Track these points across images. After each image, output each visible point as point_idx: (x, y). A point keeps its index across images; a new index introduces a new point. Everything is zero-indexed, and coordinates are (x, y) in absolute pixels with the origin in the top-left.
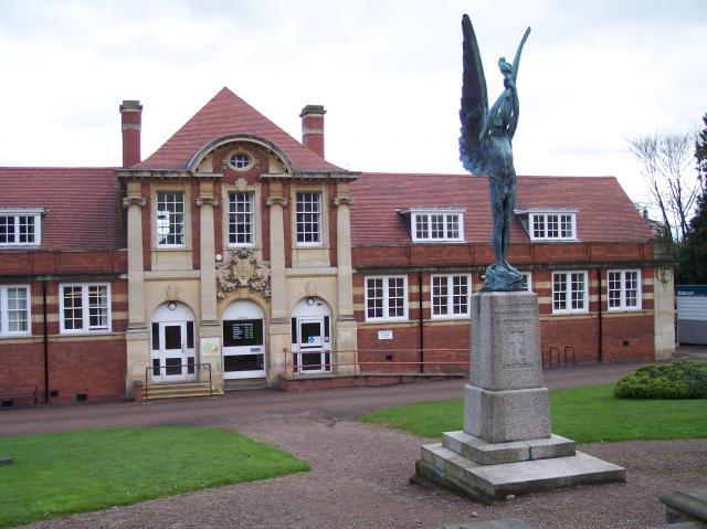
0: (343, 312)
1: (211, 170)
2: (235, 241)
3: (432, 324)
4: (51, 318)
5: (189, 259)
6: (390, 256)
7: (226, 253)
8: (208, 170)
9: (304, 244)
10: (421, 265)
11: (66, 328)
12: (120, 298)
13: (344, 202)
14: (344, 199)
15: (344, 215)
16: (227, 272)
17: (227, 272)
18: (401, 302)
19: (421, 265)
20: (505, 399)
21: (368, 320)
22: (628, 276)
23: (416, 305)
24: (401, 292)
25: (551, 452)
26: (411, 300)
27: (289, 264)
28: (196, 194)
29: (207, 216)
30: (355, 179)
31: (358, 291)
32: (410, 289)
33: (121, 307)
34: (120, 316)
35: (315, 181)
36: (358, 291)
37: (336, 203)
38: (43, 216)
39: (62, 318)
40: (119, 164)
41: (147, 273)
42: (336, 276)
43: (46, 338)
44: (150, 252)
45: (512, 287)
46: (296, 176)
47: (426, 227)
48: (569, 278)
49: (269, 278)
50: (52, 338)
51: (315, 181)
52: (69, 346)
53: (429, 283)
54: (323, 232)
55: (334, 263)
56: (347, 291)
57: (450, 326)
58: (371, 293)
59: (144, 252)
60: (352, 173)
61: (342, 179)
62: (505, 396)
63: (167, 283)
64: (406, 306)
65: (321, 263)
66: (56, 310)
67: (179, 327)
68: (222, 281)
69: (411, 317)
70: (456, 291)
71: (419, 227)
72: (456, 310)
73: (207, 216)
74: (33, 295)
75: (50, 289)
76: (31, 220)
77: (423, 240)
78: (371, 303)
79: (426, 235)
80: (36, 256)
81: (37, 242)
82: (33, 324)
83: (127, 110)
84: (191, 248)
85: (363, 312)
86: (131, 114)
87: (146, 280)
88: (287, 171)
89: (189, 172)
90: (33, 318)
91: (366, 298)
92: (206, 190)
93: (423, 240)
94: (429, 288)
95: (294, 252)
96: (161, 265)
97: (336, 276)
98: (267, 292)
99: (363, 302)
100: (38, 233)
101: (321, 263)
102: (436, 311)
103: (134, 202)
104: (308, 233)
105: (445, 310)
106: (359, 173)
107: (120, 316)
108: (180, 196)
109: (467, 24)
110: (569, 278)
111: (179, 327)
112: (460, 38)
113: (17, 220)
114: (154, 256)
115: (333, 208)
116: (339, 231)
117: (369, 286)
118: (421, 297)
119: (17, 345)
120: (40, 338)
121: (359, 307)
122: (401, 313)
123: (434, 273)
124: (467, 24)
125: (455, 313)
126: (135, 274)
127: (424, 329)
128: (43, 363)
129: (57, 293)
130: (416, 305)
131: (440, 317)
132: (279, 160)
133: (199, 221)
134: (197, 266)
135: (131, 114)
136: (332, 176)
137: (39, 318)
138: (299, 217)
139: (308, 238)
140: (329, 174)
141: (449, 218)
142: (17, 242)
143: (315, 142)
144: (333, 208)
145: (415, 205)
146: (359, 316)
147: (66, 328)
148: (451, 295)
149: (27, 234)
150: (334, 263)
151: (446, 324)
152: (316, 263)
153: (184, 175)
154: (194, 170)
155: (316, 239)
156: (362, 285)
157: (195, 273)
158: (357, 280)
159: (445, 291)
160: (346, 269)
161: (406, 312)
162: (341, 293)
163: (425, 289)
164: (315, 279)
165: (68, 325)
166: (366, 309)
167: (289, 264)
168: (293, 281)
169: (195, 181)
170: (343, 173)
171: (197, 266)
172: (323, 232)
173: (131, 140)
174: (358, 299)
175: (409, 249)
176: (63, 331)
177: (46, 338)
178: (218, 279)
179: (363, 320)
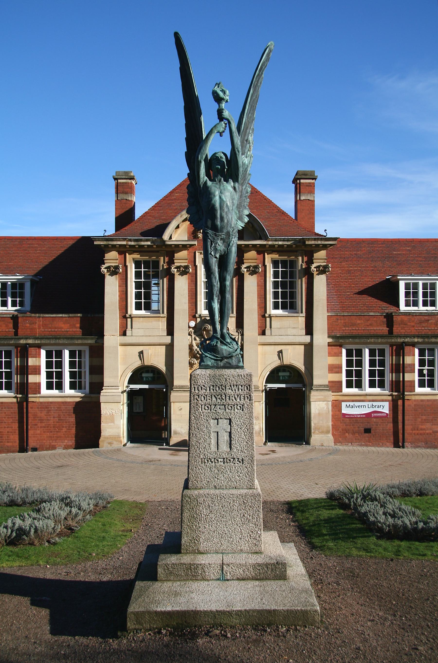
3: (413, 398)
11: (370, 387)
13: (322, 270)
15: (320, 283)
18: (382, 374)
20: (201, 500)
21: (345, 390)
25: (251, 573)
39: (43, 379)
45: (221, 364)
48: (66, 353)
50: (32, 398)
52: (46, 406)
55: (309, 330)
58: (349, 363)
62: (199, 496)
65: (294, 332)
66: (37, 370)
67: (370, 387)
68: (195, 347)
71: (407, 294)
75: (32, 350)
77: (412, 309)
78: (349, 373)
85: (341, 382)
86: (123, 186)
91: (417, 367)
93: (412, 309)
101: (294, 332)
102: (349, 385)
107: (96, 379)
109: (176, 35)
110: (66, 353)
111: (370, 387)
124: (176, 35)
129: (39, 356)
135: (123, 186)
143: (305, 208)
145: (403, 274)
147: (370, 387)
152: (290, 331)
161: (387, 384)
163: (408, 360)
165: (49, 386)
166: (417, 378)
176: (44, 391)
178: (191, 347)
179: (340, 389)
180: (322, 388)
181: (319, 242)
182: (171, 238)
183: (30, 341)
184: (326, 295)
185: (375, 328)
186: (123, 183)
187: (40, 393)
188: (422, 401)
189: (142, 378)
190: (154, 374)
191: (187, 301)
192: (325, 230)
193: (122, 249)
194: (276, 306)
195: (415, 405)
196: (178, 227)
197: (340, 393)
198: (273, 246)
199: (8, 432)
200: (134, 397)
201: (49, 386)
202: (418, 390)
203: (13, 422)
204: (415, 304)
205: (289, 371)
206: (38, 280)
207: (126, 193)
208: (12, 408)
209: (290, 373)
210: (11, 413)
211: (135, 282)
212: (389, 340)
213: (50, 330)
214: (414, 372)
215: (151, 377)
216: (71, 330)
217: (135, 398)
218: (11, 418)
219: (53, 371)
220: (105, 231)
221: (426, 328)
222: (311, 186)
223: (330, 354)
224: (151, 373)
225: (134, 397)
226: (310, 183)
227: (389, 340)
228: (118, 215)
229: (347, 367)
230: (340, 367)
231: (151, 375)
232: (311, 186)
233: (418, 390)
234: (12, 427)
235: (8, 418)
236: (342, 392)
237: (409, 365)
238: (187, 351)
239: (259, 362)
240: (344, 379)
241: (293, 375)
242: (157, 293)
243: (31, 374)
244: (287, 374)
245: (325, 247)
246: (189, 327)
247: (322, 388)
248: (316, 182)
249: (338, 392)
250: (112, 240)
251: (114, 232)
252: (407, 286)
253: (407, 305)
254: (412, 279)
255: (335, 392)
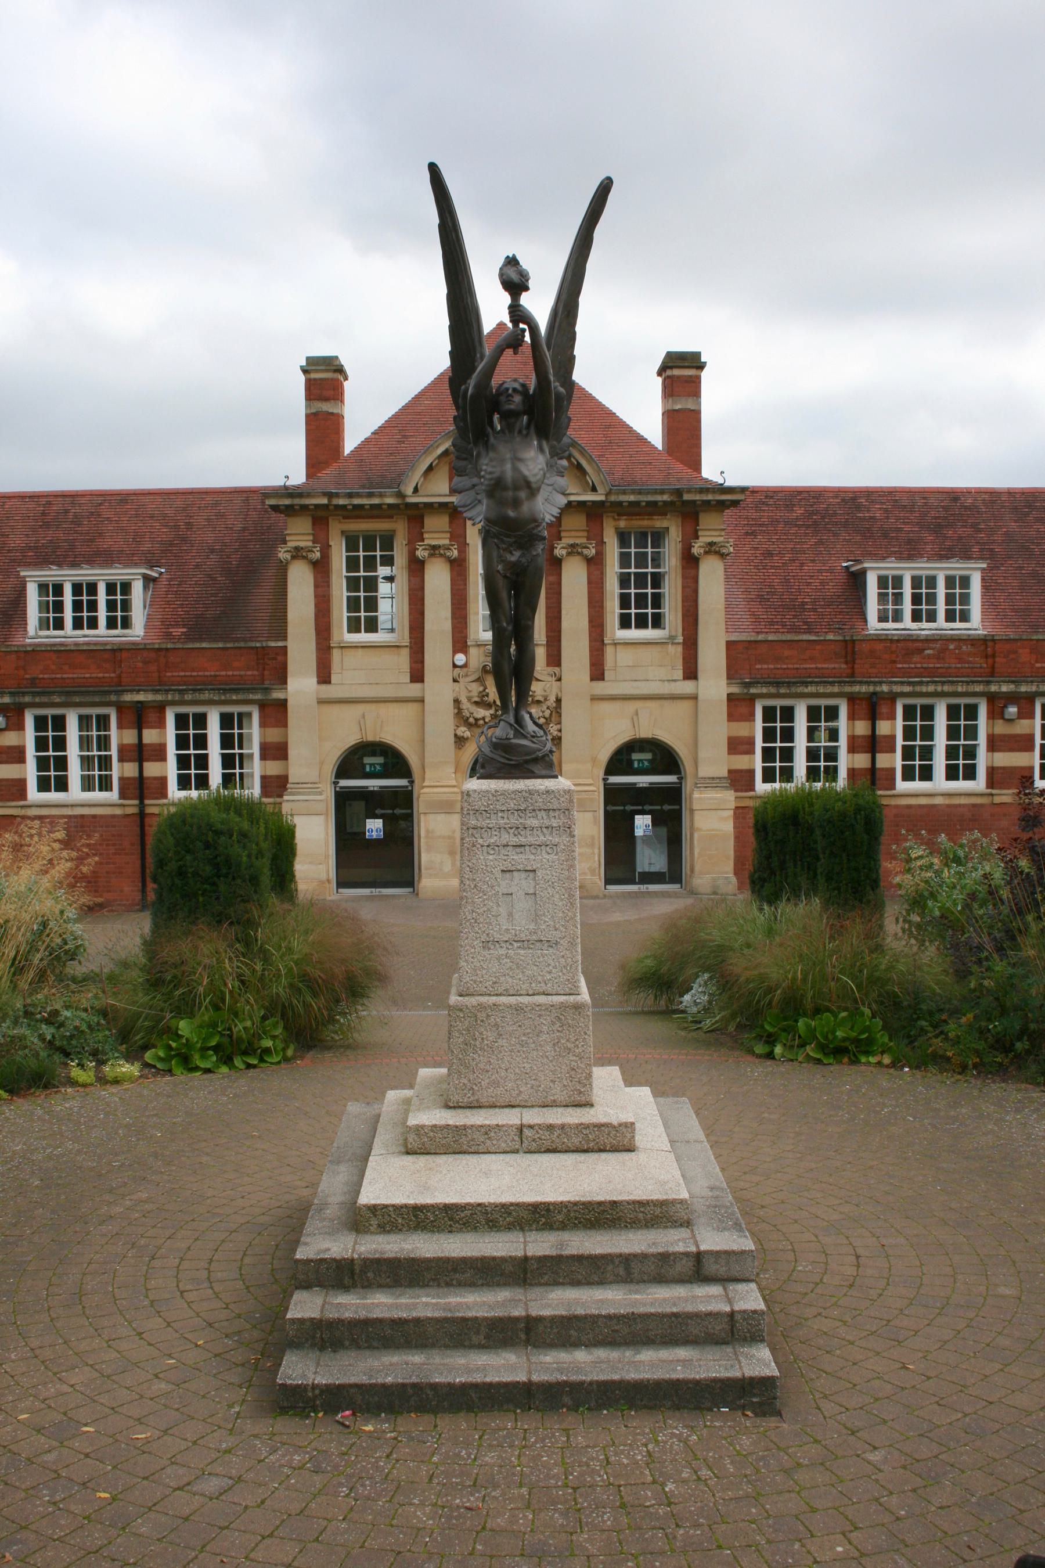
0: (705, 771)
1: (446, 490)
2: (629, 627)
3: (893, 802)
4: (151, 769)
5: (403, 659)
6: (812, 659)
7: (473, 651)
8: (439, 490)
9: (634, 634)
10: (870, 677)
11: (765, 781)
12: (274, 735)
13: (712, 549)
14: (711, 544)
15: (712, 578)
16: (476, 688)
17: (476, 688)
18: (971, 753)
19: (870, 677)
21: (762, 787)
22: (226, 721)
23: (862, 761)
24: (972, 733)
26: (852, 749)
27: (598, 673)
28: (416, 536)
29: (438, 580)
30: (735, 503)
31: (741, 730)
32: (851, 727)
33: (275, 751)
34: (274, 768)
35: (654, 509)
36: (741, 730)
37: (696, 550)
38: (147, 580)
40: (298, 476)
41: (324, 687)
42: (694, 698)
43: (142, 806)
44: (329, 648)
46: (613, 498)
47: (93, 606)
49: (559, 701)
50: (153, 806)
51: (654, 509)
53: (892, 717)
54: (672, 611)
56: (716, 728)
57: (934, 806)
58: (769, 735)
59: (319, 649)
60: (731, 490)
61: (708, 502)
63: (361, 708)
64: (116, 772)
66: (159, 753)
68: (466, 705)
69: (123, 795)
70: (953, 733)
72: (952, 774)
73: (438, 580)
74: (120, 726)
76: (126, 588)
79: (932, 617)
80: (124, 655)
81: (138, 630)
82: (121, 779)
83: (676, 372)
84: (406, 641)
86: (324, 380)
87: (321, 702)
88: (594, 489)
89: (401, 495)
90: (264, 768)
91: (759, 744)
92: (437, 531)
94: (895, 727)
95: (609, 651)
96: (351, 674)
97: (694, 698)
98: (553, 729)
99: (752, 752)
100: (138, 615)
102: (908, 774)
103: (298, 554)
104: (643, 610)
105: (927, 774)
106: (743, 490)
107: (274, 768)
108: (388, 543)
112: (436, 220)
113: (102, 589)
114: (336, 654)
115: (690, 562)
116: (700, 612)
117: (178, 727)
118: (873, 744)
119: (94, 816)
120: (132, 806)
121: (741, 762)
122: (970, 773)
123: (173, 703)
125: (84, 790)
126: (300, 685)
127: (147, 820)
128: (137, 848)
130: (862, 761)
131: (917, 785)
132: (579, 467)
133: (422, 589)
134: (417, 676)
135: (324, 380)
136: (686, 497)
137: (131, 770)
138: (624, 581)
139: (642, 623)
140: (679, 492)
141: (950, 582)
142: (907, 622)
143: (684, 427)
144: (690, 562)
146: (741, 780)
148: (940, 741)
149: (120, 619)
150: (691, 673)
151: (923, 801)
153: (390, 501)
154: (409, 490)
155: (657, 622)
156: (751, 717)
157: (414, 690)
158: (738, 707)
159: (928, 733)
160: (714, 685)
162: (703, 729)
164: (373, 706)
166: (899, 764)
167: (598, 673)
168: (335, 710)
169: (416, 515)
170: (707, 490)
171: (417, 676)
172: (672, 611)
173: (323, 431)
174: (739, 746)
175: (851, 650)
176: (174, 792)
177: (142, 806)
178: (457, 702)
179: (751, 787)
180: (712, 783)
181: (710, 497)
182: (416, 490)
183: (27, 699)
184: (723, 600)
185: (819, 666)
186: (321, 379)
187: (165, 796)
188: (909, 807)
189: (364, 766)
190: (386, 757)
191: (449, 615)
192: (722, 472)
193: (320, 513)
194: (625, 622)
195: (896, 816)
196: (430, 468)
197: (751, 793)
198: (637, 504)
199: (107, 873)
200: (347, 803)
201: (44, 785)
202: (902, 786)
203: (115, 854)
204: (898, 617)
205: (650, 751)
206: (156, 575)
207: (326, 399)
208: (114, 826)
209: (654, 754)
210: (113, 835)
211: (347, 578)
212: (847, 689)
213: (182, 674)
214: (754, 753)
215: (380, 764)
216: (223, 673)
217: (350, 805)
218: (114, 845)
219: (190, 755)
220: (287, 477)
221: (919, 666)
222: (694, 382)
223: (731, 717)
224: (381, 755)
225: (347, 803)
226: (691, 376)
227: (847, 689)
228: (574, 411)
229: (177, 749)
230: (751, 742)
231: (380, 760)
232: (694, 382)
233: (902, 786)
234: (114, 863)
235: (107, 845)
236: (894, 789)
237: (885, 737)
238: (451, 710)
239: (589, 732)
240: (758, 765)
241: (658, 757)
242: (390, 601)
243: (148, 760)
244: (648, 756)
245: (722, 506)
246: (455, 666)
247: (712, 783)
248: (704, 375)
249: (746, 791)
250: (301, 495)
251: (304, 480)
252: (882, 582)
253: (883, 618)
254: (891, 567)
255: (741, 791)
